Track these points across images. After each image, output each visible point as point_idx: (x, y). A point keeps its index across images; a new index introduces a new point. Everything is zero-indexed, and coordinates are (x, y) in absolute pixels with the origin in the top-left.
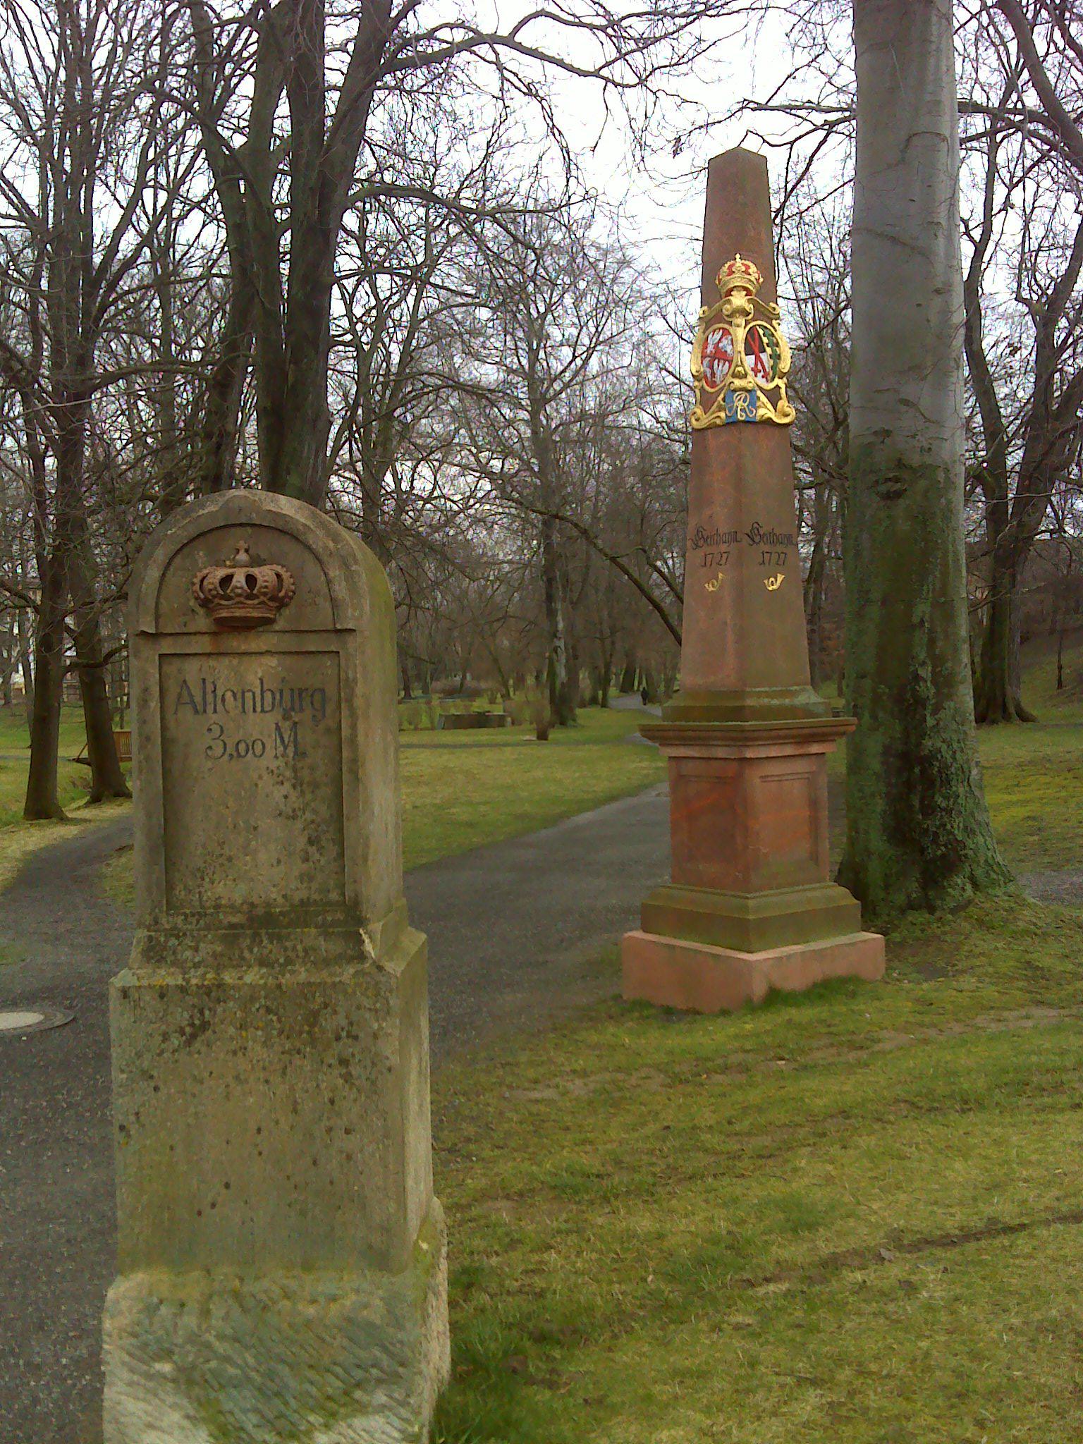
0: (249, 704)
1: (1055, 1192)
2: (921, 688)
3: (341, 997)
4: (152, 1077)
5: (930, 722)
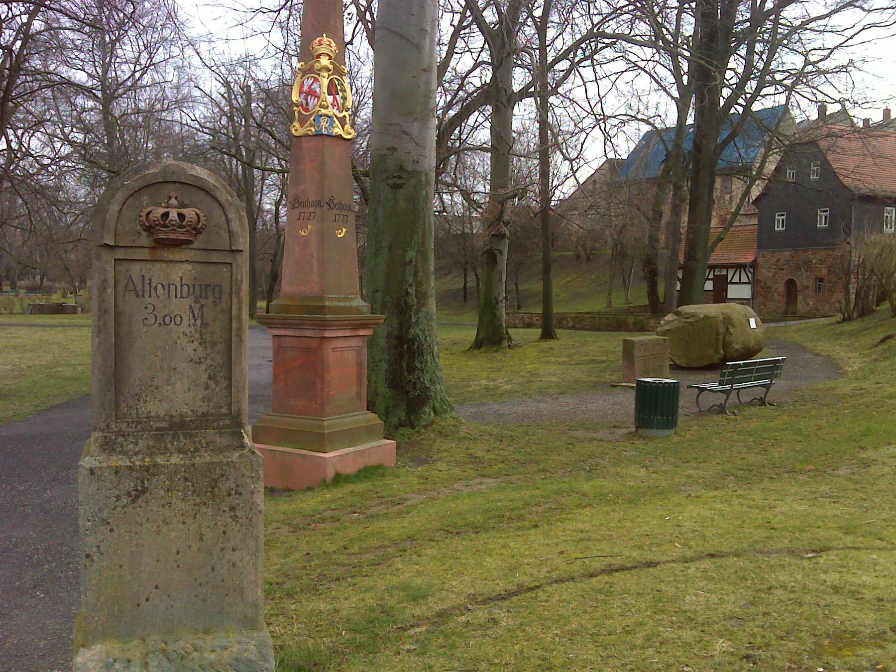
0: (173, 293)
1: (545, 569)
3: (232, 470)
4: (108, 523)
5: (414, 319)
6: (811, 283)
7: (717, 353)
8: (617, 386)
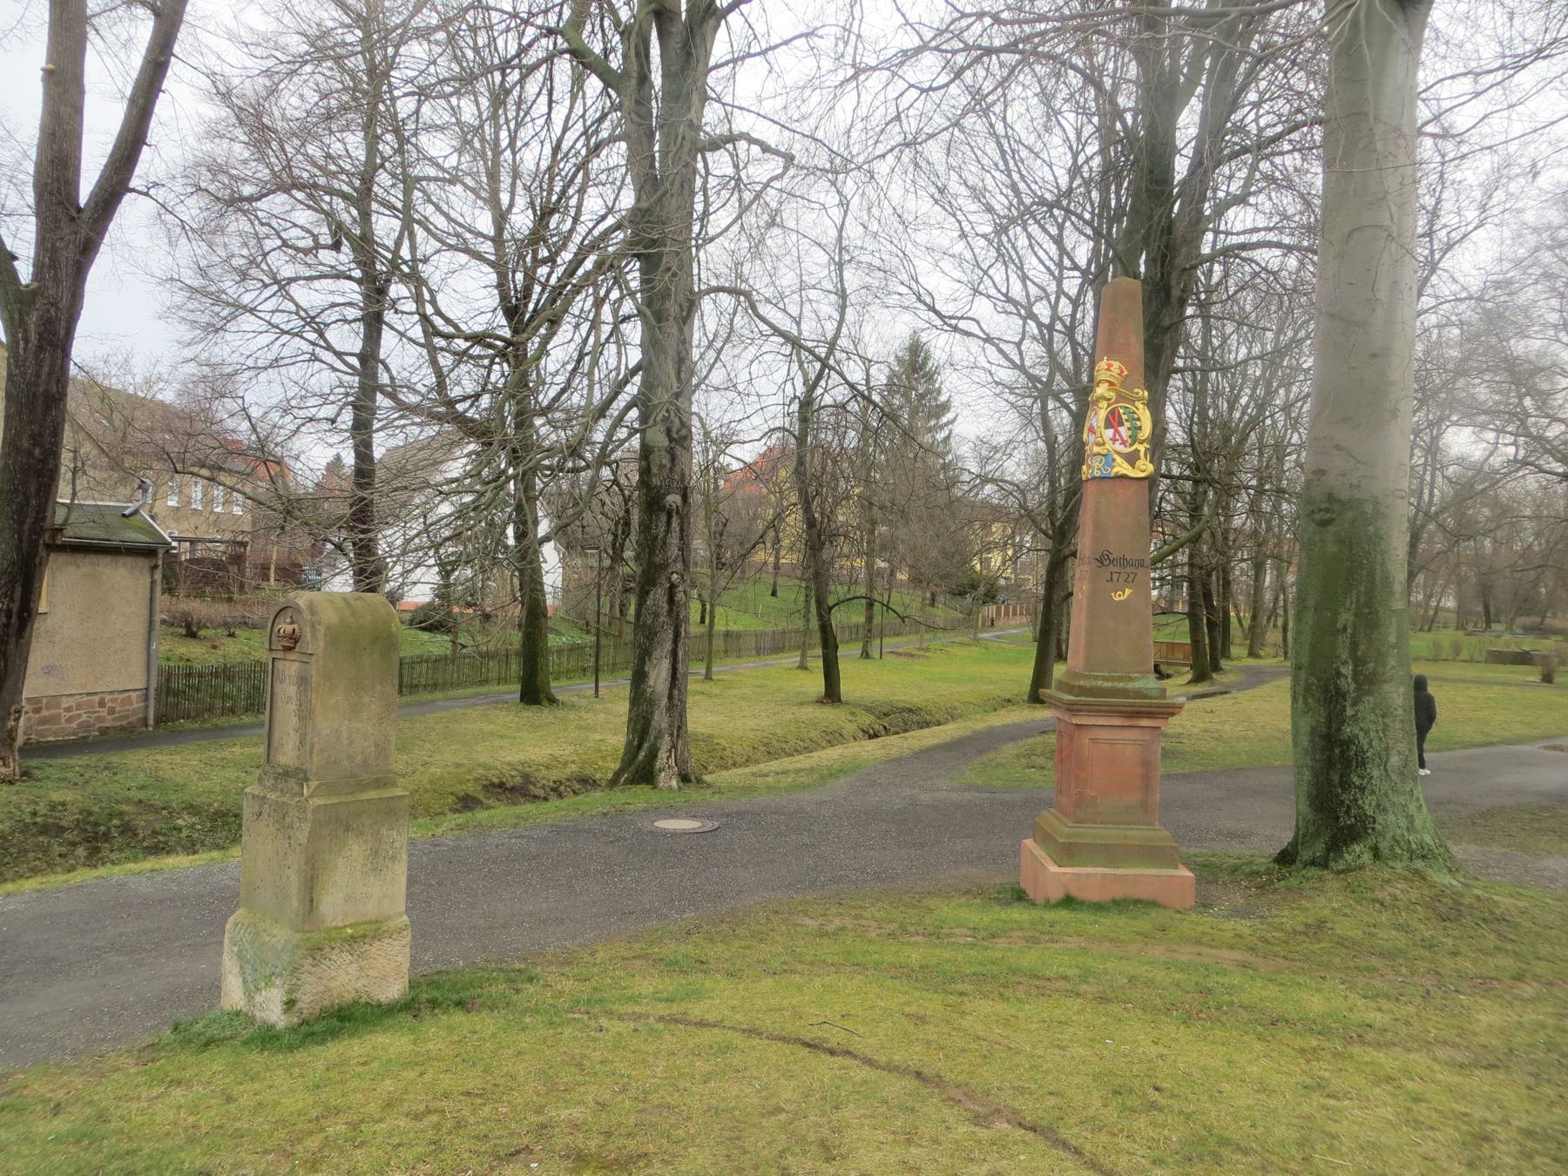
2: (1342, 682)
5: (1349, 712)
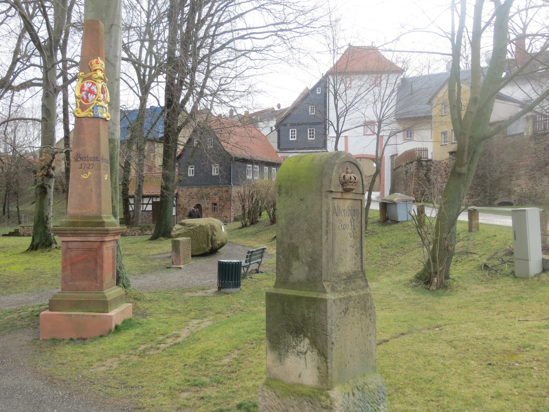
6: (210, 206)
7: (208, 246)
8: (170, 268)
